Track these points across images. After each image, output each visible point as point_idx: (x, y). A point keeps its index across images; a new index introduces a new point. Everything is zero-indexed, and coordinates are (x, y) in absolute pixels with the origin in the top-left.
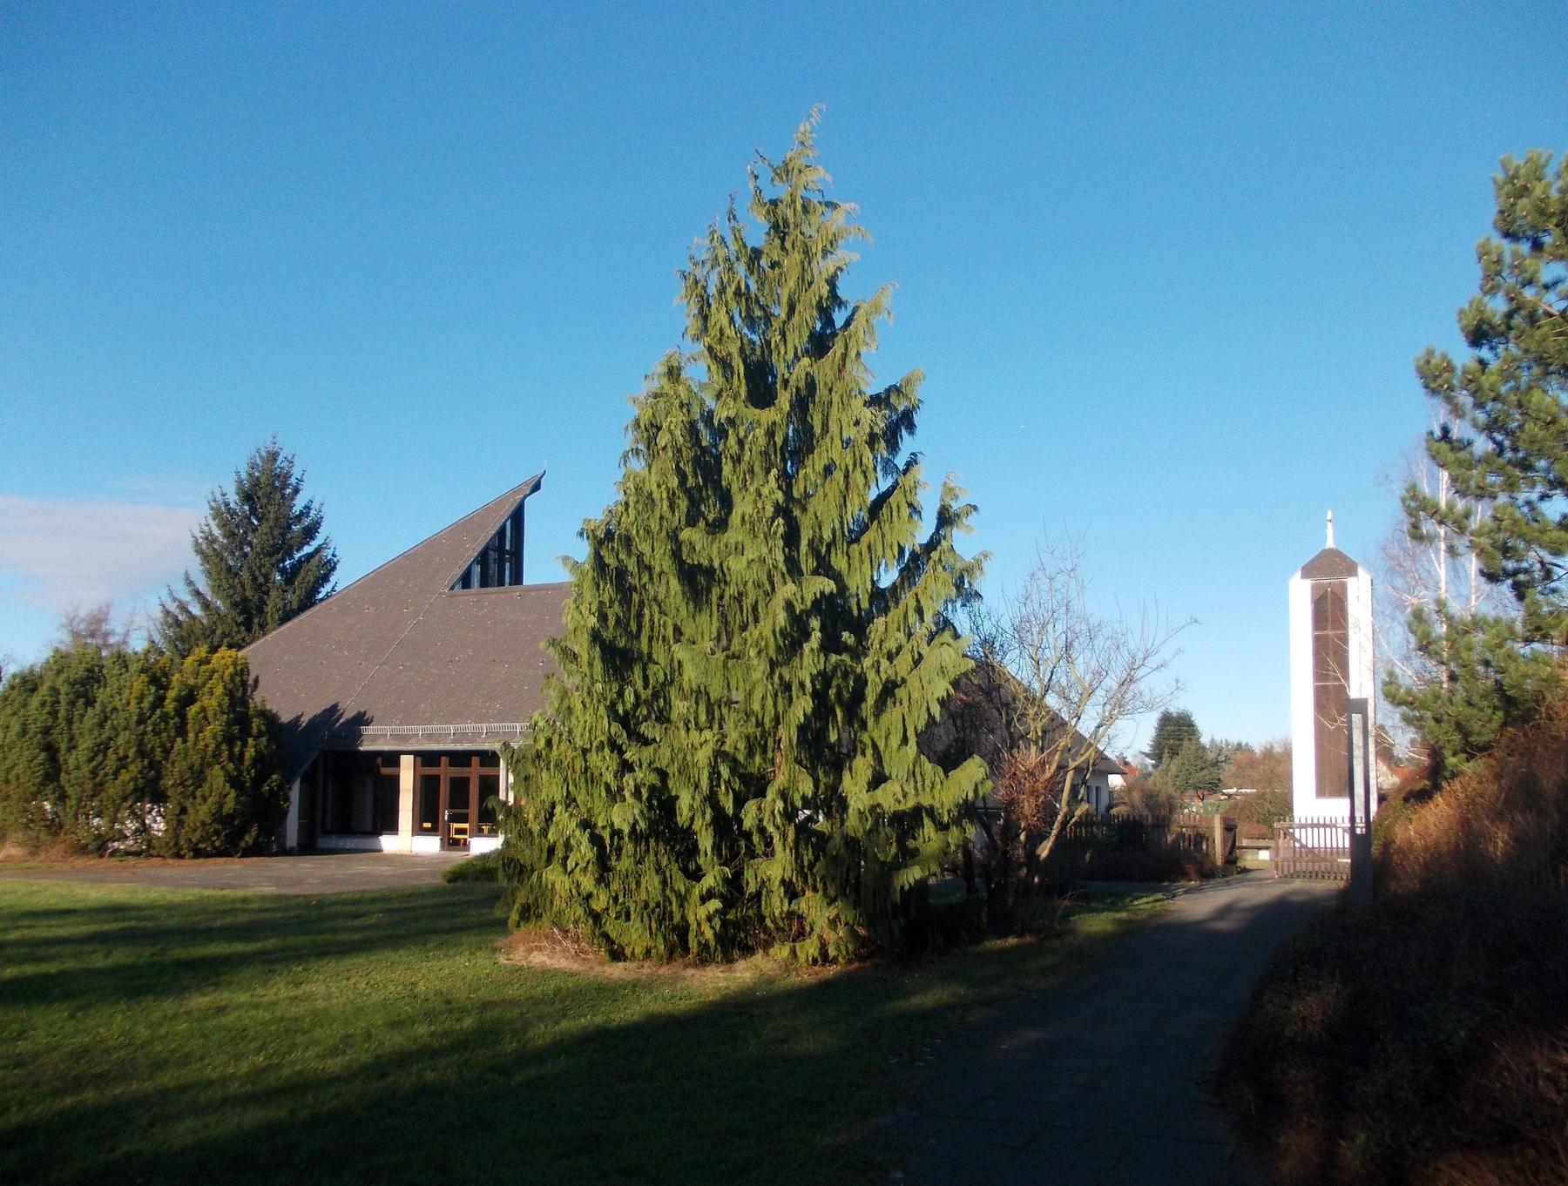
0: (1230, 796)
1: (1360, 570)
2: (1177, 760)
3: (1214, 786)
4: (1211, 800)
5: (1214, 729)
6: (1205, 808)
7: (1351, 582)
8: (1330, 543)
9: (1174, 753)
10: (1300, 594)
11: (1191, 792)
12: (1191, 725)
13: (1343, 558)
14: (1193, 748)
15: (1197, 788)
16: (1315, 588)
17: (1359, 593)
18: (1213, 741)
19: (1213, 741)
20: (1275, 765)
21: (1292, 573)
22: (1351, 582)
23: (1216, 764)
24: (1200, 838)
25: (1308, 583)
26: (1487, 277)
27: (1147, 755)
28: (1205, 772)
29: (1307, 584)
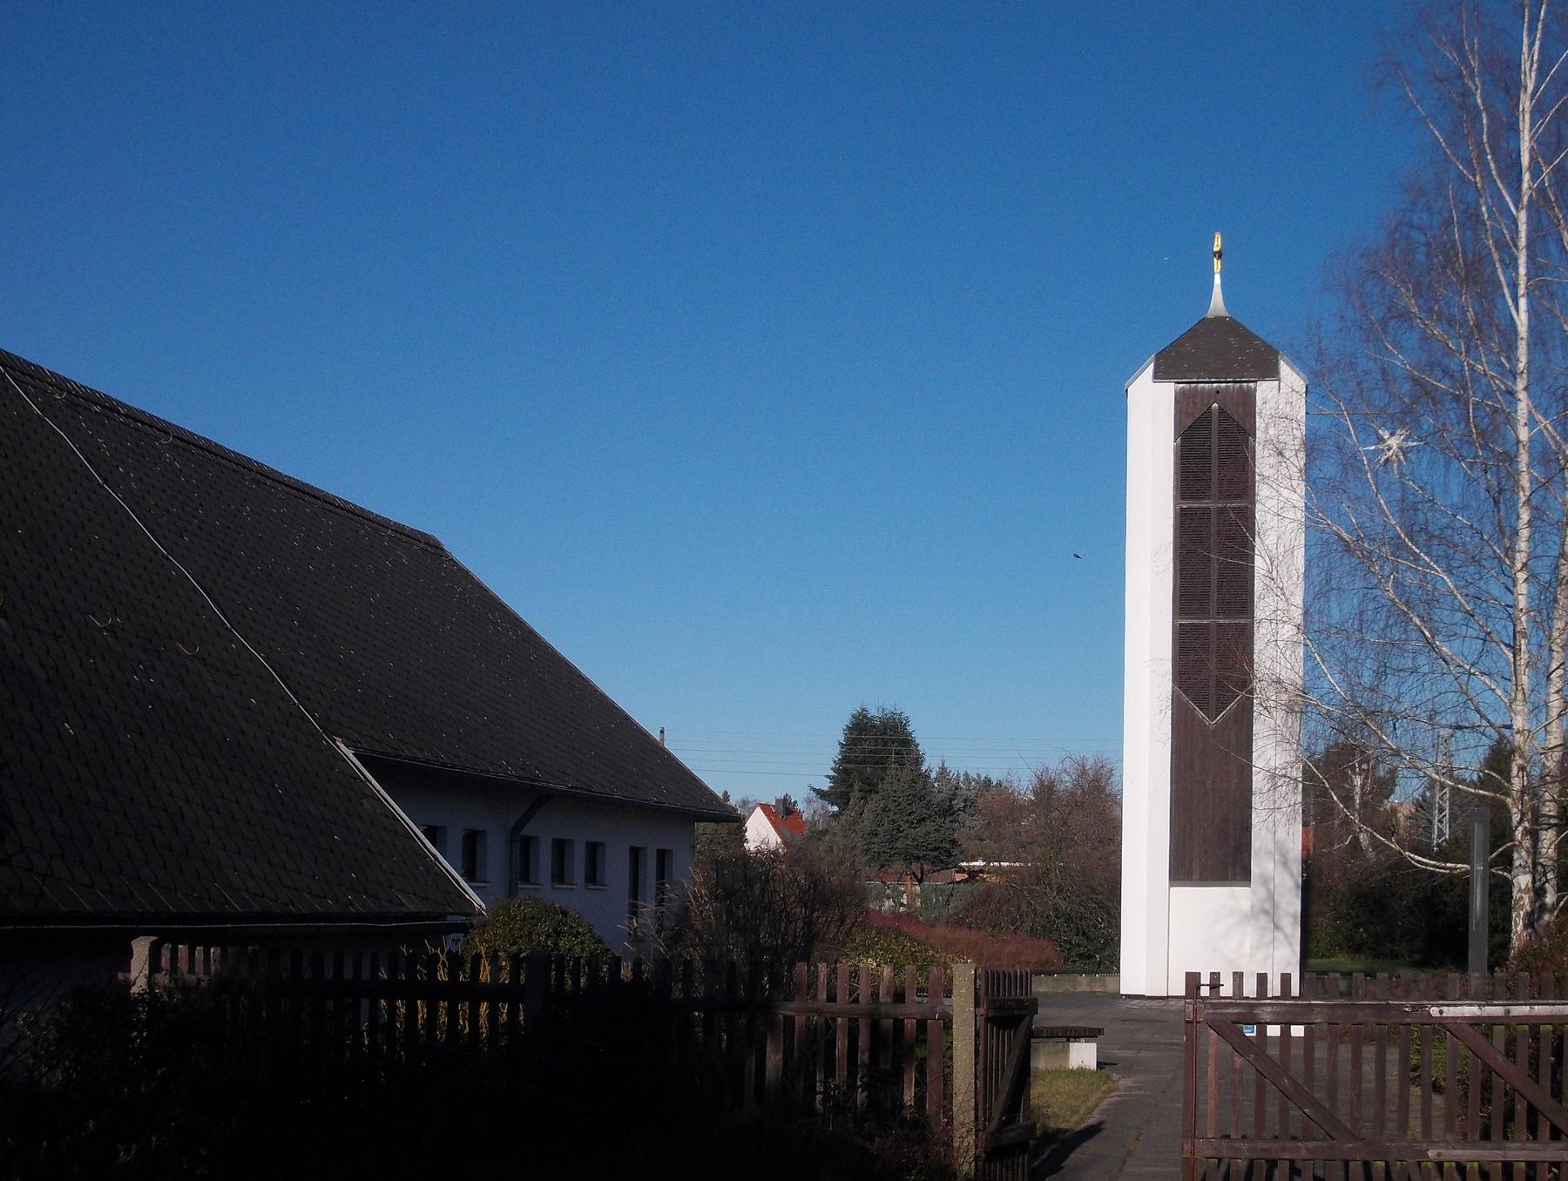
0: (973, 874)
1: (1285, 369)
2: (875, 803)
3: (944, 855)
4: (938, 881)
5: (953, 747)
6: (924, 896)
7: (1264, 391)
8: (1217, 303)
9: (870, 788)
10: (1151, 410)
11: (898, 866)
12: (907, 742)
13: (1247, 337)
14: (906, 776)
15: (909, 858)
16: (1180, 399)
17: (1280, 403)
18: (943, 771)
19: (943, 771)
20: (1090, 810)
21: (1132, 371)
22: (1264, 391)
23: (947, 811)
24: (899, 1045)
25: (1168, 390)
26: (1492, 952)
27: (822, 794)
28: (929, 826)
29: (1167, 391)
